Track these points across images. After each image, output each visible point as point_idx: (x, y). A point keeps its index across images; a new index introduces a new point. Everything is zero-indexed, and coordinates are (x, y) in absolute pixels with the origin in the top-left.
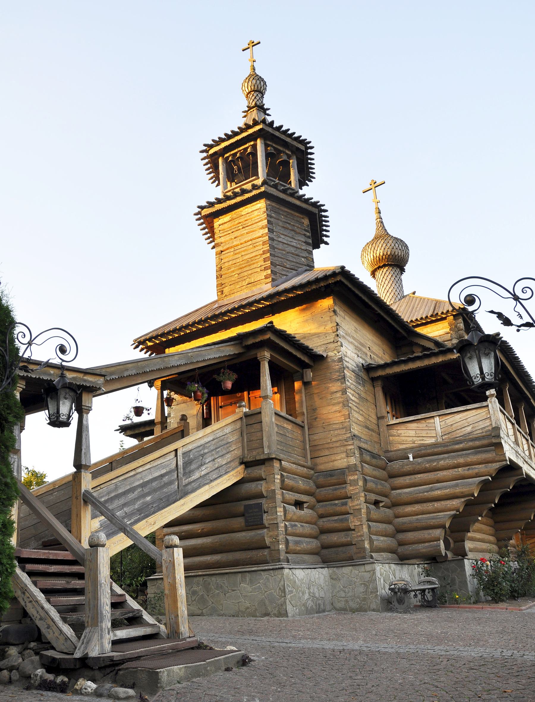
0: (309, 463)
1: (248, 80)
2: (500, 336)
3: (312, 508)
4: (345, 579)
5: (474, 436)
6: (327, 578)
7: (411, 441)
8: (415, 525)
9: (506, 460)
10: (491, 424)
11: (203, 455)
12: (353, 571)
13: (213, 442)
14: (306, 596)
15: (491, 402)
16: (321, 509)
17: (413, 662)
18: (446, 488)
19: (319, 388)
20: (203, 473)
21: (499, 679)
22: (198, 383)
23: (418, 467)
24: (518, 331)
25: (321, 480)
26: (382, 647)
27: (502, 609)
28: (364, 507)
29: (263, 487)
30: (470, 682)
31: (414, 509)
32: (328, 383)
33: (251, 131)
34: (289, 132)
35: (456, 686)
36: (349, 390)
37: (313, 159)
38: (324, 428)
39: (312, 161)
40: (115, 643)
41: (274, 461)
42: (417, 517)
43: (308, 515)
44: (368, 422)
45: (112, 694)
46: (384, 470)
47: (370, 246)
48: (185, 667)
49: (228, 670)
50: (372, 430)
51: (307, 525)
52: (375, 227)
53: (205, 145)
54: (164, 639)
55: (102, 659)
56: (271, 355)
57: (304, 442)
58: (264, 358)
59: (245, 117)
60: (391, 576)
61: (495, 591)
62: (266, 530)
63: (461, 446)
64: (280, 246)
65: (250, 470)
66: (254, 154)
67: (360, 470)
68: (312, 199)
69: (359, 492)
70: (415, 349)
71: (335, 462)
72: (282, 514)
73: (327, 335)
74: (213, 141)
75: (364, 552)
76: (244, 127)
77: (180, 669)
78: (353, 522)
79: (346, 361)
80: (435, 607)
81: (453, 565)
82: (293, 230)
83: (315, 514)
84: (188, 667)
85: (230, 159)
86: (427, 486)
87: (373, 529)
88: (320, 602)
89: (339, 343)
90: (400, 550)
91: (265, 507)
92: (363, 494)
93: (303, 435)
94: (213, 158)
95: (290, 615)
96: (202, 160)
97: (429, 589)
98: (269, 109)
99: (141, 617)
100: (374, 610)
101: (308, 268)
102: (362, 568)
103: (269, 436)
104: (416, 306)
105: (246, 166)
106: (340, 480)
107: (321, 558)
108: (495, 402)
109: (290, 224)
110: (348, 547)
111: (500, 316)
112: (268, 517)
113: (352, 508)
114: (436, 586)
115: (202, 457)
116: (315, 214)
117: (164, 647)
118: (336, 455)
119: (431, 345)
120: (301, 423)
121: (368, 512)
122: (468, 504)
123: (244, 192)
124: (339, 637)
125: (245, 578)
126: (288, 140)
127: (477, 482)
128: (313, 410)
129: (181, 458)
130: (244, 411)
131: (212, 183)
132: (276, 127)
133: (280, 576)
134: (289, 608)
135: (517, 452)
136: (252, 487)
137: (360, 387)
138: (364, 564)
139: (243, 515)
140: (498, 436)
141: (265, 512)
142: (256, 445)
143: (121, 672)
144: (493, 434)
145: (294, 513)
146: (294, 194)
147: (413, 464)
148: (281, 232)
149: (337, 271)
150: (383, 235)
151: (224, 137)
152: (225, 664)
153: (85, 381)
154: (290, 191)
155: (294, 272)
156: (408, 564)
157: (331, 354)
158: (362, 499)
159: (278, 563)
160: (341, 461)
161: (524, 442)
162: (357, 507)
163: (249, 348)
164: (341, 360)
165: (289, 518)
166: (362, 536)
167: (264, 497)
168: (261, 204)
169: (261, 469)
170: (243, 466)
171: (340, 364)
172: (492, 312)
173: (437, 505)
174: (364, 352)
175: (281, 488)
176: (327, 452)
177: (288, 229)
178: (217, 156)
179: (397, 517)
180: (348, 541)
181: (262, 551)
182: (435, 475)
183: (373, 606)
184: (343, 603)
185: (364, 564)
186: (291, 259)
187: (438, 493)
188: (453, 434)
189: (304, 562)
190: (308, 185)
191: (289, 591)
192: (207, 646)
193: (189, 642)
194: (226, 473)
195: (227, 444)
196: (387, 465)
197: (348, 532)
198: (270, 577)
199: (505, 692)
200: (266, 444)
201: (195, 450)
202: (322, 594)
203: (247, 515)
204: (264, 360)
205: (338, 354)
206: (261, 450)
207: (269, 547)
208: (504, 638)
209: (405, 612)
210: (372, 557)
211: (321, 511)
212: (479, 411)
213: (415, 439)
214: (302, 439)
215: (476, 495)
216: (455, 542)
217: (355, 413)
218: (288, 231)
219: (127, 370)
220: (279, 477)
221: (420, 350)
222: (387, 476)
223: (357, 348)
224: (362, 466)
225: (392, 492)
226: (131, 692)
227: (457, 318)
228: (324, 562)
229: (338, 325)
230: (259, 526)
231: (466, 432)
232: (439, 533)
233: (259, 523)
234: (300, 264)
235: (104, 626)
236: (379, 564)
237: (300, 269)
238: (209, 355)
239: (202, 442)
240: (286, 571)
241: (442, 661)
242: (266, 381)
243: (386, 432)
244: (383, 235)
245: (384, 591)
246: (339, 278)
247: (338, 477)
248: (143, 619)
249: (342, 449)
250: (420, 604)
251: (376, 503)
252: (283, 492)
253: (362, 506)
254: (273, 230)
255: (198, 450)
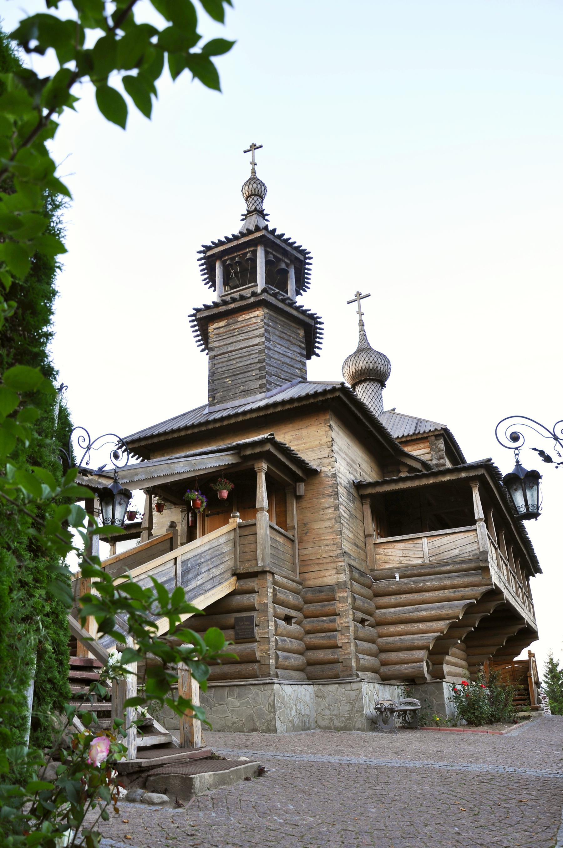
0: (298, 578)
1: (248, 183)
2: (492, 462)
3: (299, 623)
4: (330, 697)
5: (462, 559)
6: (313, 695)
7: (397, 561)
8: (399, 645)
9: (492, 585)
10: (479, 548)
11: (199, 565)
12: (339, 689)
13: (209, 552)
14: (293, 713)
15: (479, 526)
16: (308, 625)
17: (424, 775)
18: (431, 609)
19: (310, 502)
20: (199, 583)
21: (511, 791)
22: (198, 491)
23: (404, 587)
24: (557, 467)
25: (309, 596)
26: (386, 761)
27: (483, 732)
28: (352, 624)
29: (255, 600)
30: (485, 792)
31: (398, 629)
32: (320, 498)
33: (251, 237)
34: (290, 241)
35: (474, 796)
36: (341, 507)
37: (310, 270)
38: (315, 543)
39: (309, 272)
40: (140, 749)
41: (268, 574)
42: (400, 637)
43: (297, 630)
44: (357, 539)
45: (146, 800)
46: (370, 588)
47: (353, 359)
48: (214, 774)
49: (247, 779)
50: (360, 548)
51: (295, 640)
52: (357, 339)
53: (203, 246)
54: (176, 748)
55: (130, 765)
56: (268, 466)
57: (293, 556)
58: (261, 470)
59: (243, 220)
60: (376, 696)
61: (476, 714)
62: (256, 644)
63: (448, 568)
64: (276, 356)
65: (242, 582)
66: (254, 260)
67: (350, 587)
68: (310, 310)
69: (348, 610)
70: (402, 468)
71: (325, 579)
72: (273, 628)
73: (321, 450)
74: (213, 242)
75: (351, 670)
76: (245, 231)
77: (210, 776)
78: (341, 639)
79: (340, 477)
80: (416, 728)
81: (431, 687)
82: (289, 341)
83: (302, 630)
84: (218, 774)
85: (228, 262)
86: (413, 607)
87: (360, 647)
88: (305, 719)
89: (334, 459)
90: (383, 670)
91: (257, 620)
92: (351, 612)
93: (293, 548)
94: (210, 260)
95: (278, 731)
96: (198, 260)
97: (410, 710)
98: (268, 215)
99: (152, 726)
100: (359, 729)
101: (301, 380)
102: (348, 687)
103: (264, 549)
104: (396, 423)
105: (244, 271)
106: (330, 597)
107: (307, 675)
108: (483, 526)
109: (286, 334)
110: (334, 665)
111: (542, 453)
112: (259, 631)
113: (340, 625)
114: (419, 707)
115: (199, 566)
116: (312, 326)
117: (183, 756)
118: (326, 571)
119: (418, 466)
120: (291, 537)
121: (356, 630)
122: (452, 627)
123: (242, 298)
124: (338, 752)
125: (233, 692)
126: (288, 248)
127: (463, 605)
128: (304, 524)
129: (180, 566)
130: (238, 521)
131: (205, 284)
132: (278, 235)
133: (270, 691)
134: (278, 723)
135: (500, 577)
136: (243, 600)
137: (350, 504)
138: (350, 683)
139: (232, 627)
140: (486, 561)
141: (256, 626)
142: (249, 557)
143: (152, 778)
144: (481, 558)
145: (284, 629)
146: (292, 304)
147: (400, 584)
148: (278, 341)
149: (337, 387)
150: (364, 348)
151: (224, 239)
152: (245, 774)
153: (100, 483)
154: (288, 301)
155: (289, 383)
156: (390, 685)
157: (324, 469)
158: (351, 617)
159: (268, 678)
160: (330, 578)
161: (504, 567)
162: (346, 625)
163: (245, 458)
164: (335, 476)
165: (279, 632)
166: (349, 654)
167: (256, 610)
168: (259, 313)
169: (254, 582)
170: (235, 578)
171: (334, 479)
172: (535, 449)
173: (422, 626)
174: (355, 469)
175: (273, 602)
176: (317, 568)
177: (284, 339)
178: (214, 258)
179: (380, 636)
180: (335, 659)
181: (251, 665)
182: (421, 596)
183: (359, 725)
184: (328, 721)
185: (350, 683)
186: (285, 369)
187: (423, 614)
188: (440, 555)
189: (290, 678)
190: (302, 295)
191: (279, 707)
192: (219, 757)
193: (204, 752)
194: (220, 584)
195: (221, 554)
196: (372, 584)
197: (335, 650)
198: (260, 692)
199: (521, 801)
200: (260, 556)
201: (192, 559)
202: (308, 712)
203: (237, 628)
204: (262, 471)
205: (332, 470)
206: (254, 562)
207: (259, 662)
208: (500, 756)
209: (390, 732)
210: (358, 676)
211: (308, 627)
212: (467, 534)
213: (401, 559)
214: (292, 553)
215: (461, 618)
216: (433, 664)
217: (346, 529)
218: (284, 341)
219: (137, 474)
220: (271, 590)
221: (407, 470)
222: (372, 595)
223: (349, 465)
224: (352, 584)
225: (377, 611)
226: (165, 798)
227: (439, 438)
228: (309, 679)
229: (333, 440)
230: (251, 639)
231: (454, 554)
232: (422, 654)
233: (250, 636)
234: (294, 375)
235: (130, 733)
236: (366, 683)
237: (294, 381)
238: (210, 463)
239: (199, 551)
240: (276, 686)
241: (451, 775)
242: (262, 492)
243: (373, 551)
244: (364, 348)
245: (370, 710)
246: (337, 394)
247: (327, 594)
248: (154, 727)
249: (332, 565)
250: (401, 725)
251: (362, 621)
252: (274, 606)
253: (350, 624)
254: (269, 339)
255: (195, 559)
